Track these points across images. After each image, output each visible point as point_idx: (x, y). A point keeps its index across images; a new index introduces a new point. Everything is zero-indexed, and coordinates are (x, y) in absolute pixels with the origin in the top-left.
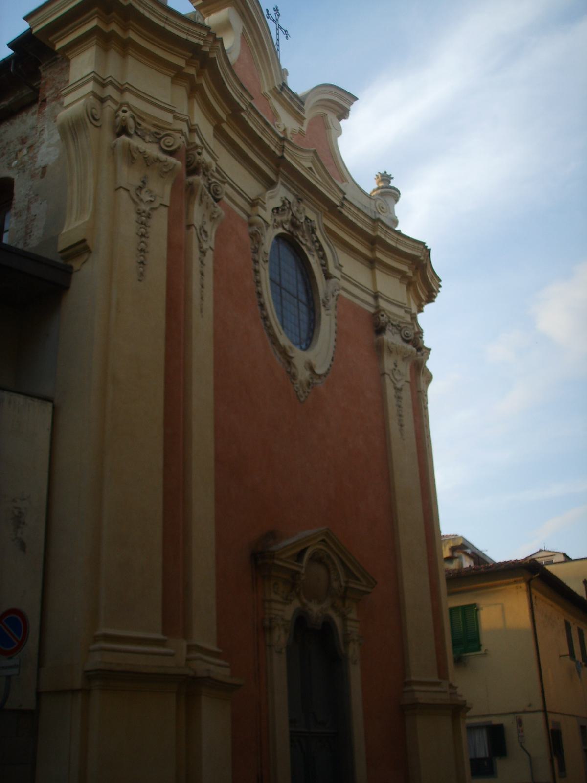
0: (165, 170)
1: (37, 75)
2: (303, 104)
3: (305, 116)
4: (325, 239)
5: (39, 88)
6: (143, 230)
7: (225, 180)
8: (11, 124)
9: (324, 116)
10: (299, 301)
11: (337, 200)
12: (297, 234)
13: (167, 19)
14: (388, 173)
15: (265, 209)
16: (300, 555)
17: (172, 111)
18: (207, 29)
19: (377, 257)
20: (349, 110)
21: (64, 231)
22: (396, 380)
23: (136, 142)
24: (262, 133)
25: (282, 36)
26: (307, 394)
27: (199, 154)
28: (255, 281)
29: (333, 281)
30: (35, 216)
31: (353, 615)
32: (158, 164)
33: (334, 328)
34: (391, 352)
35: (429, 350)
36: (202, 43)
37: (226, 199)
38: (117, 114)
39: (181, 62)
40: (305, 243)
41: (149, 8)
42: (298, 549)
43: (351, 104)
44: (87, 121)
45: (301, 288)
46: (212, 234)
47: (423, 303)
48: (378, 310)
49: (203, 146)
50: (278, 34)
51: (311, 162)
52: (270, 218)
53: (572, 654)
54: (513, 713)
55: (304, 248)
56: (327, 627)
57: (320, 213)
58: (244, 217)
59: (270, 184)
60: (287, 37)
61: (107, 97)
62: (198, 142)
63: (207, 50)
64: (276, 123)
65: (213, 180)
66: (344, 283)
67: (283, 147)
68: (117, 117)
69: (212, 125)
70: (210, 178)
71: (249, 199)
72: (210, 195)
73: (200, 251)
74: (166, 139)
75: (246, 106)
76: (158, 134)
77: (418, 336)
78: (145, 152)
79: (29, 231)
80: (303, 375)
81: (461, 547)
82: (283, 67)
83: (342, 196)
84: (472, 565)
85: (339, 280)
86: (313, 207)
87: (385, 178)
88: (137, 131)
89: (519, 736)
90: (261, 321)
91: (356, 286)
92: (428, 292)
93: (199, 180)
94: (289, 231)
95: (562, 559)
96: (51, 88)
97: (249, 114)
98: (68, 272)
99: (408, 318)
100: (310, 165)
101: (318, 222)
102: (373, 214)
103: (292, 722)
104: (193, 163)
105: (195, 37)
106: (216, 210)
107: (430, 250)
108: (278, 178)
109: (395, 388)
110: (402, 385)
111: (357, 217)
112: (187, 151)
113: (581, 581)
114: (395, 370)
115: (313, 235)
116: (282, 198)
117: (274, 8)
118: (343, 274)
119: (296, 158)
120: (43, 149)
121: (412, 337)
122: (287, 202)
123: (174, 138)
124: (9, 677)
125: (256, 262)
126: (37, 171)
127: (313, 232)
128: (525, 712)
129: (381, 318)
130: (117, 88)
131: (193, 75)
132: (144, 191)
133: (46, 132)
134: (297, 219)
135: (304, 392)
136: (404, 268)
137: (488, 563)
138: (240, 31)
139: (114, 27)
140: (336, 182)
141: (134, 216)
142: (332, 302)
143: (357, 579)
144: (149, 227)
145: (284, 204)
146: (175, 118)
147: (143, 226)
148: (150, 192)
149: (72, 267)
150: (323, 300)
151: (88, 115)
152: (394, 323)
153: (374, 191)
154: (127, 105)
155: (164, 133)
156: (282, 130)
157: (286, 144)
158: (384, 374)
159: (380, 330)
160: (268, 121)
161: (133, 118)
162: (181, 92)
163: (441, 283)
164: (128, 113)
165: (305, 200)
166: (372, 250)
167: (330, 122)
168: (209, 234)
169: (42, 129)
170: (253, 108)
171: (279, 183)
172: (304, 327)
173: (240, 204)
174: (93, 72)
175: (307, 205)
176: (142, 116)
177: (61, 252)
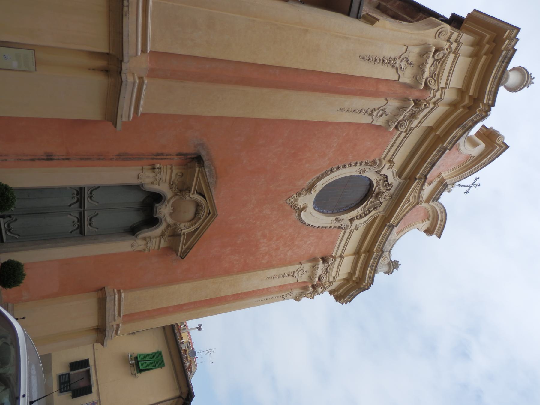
4: (371, 217)
6: (386, 61)
11: (393, 222)
14: (400, 267)
19: (362, 255)
24: (429, 162)
26: (291, 205)
27: (321, 289)
28: (351, 163)
35: (313, 299)
40: (368, 204)
54: (100, 400)
67: (421, 179)
69: (335, 288)
70: (409, 121)
71: (459, 39)
78: (427, 63)
83: (395, 225)
85: (350, 229)
86: (388, 206)
90: (330, 168)
94: (375, 191)
100: (411, 201)
106: (393, 123)
107: (369, 289)
109: (294, 272)
115: (372, 209)
118: (353, 230)
122: (390, 187)
129: (331, 259)
134: (381, 196)
136: (357, 274)
141: (393, 57)
142: (338, 225)
144: (388, 66)
145: (389, 185)
152: (328, 269)
154: (335, 261)
159: (325, 260)
166: (364, 252)
173: (389, 154)
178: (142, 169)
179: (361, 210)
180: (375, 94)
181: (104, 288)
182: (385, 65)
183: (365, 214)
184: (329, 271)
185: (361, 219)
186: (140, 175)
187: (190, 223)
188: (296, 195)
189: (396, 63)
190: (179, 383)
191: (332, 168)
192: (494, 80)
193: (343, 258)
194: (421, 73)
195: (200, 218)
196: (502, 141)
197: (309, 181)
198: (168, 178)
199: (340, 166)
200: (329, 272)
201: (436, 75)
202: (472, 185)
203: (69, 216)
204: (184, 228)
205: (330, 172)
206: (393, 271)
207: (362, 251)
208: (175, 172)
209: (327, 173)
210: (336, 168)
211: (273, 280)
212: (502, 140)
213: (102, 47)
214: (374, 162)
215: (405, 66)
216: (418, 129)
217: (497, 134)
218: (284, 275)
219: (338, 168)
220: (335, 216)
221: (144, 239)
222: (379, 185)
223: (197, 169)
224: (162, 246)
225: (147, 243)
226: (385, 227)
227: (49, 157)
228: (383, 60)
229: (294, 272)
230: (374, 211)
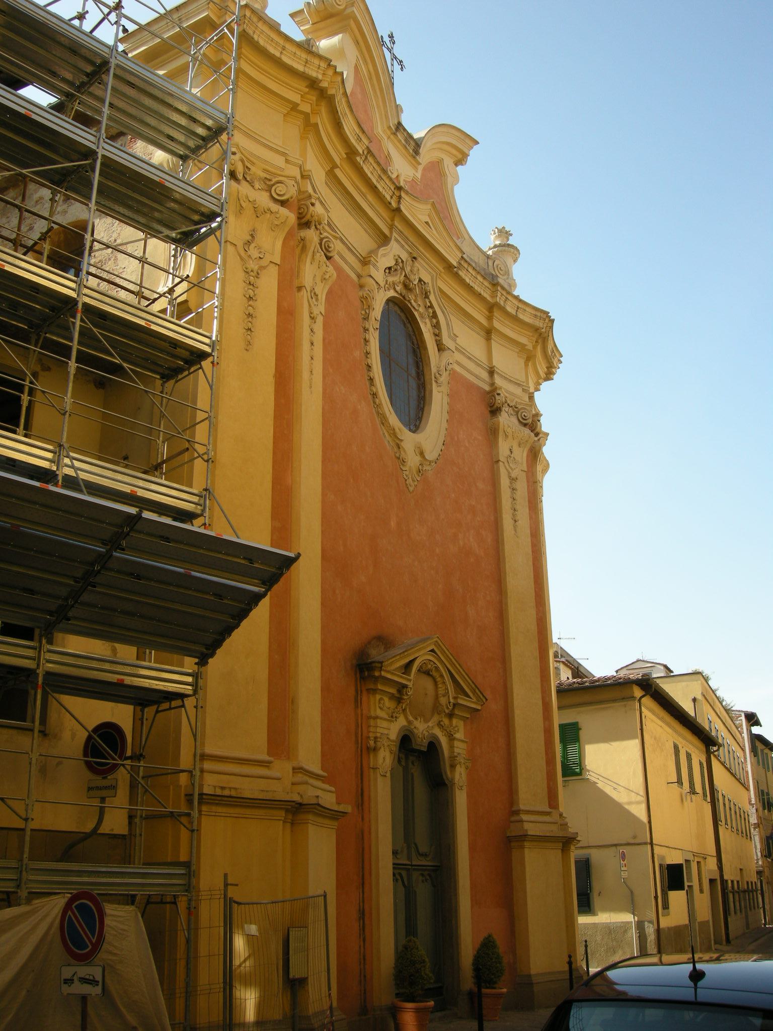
7: (337, 236)
12: (409, 298)
15: (377, 270)
16: (408, 666)
17: (284, 154)
26: (416, 483)
27: (313, 205)
29: (446, 354)
31: (459, 735)
32: (268, 215)
35: (547, 435)
36: (320, 77)
37: (337, 258)
45: (411, 360)
46: (322, 297)
48: (493, 391)
51: (429, 216)
53: (680, 782)
55: (416, 313)
56: (433, 746)
58: (353, 276)
62: (310, 190)
66: (458, 356)
69: (325, 170)
73: (311, 317)
74: (278, 187)
76: (270, 180)
77: (536, 419)
80: (413, 460)
82: (398, 103)
83: (460, 255)
91: (469, 358)
92: (547, 368)
93: (311, 234)
101: (433, 286)
103: (395, 853)
104: (306, 215)
107: (553, 321)
109: (510, 477)
112: (299, 201)
114: (510, 457)
115: (427, 300)
116: (395, 256)
121: (530, 421)
123: (287, 186)
125: (366, 330)
127: (427, 297)
128: (628, 844)
129: (497, 397)
132: (253, 245)
135: (413, 481)
136: (523, 340)
137: (594, 677)
138: (354, 62)
140: (454, 238)
141: (241, 275)
142: (444, 378)
143: (468, 696)
144: (257, 288)
146: (287, 161)
147: (251, 287)
148: (259, 248)
153: (490, 249)
155: (277, 179)
158: (498, 461)
159: (495, 411)
161: (242, 161)
167: (446, 166)
168: (319, 297)
171: (393, 238)
172: (413, 404)
175: (423, 266)
176: (252, 159)
182: (255, 295)
187: (440, 686)
188: (404, 472)
190: (614, 700)
195: (437, 668)
199: (368, 376)
201: (268, 177)
204: (447, 697)
224: (463, 738)
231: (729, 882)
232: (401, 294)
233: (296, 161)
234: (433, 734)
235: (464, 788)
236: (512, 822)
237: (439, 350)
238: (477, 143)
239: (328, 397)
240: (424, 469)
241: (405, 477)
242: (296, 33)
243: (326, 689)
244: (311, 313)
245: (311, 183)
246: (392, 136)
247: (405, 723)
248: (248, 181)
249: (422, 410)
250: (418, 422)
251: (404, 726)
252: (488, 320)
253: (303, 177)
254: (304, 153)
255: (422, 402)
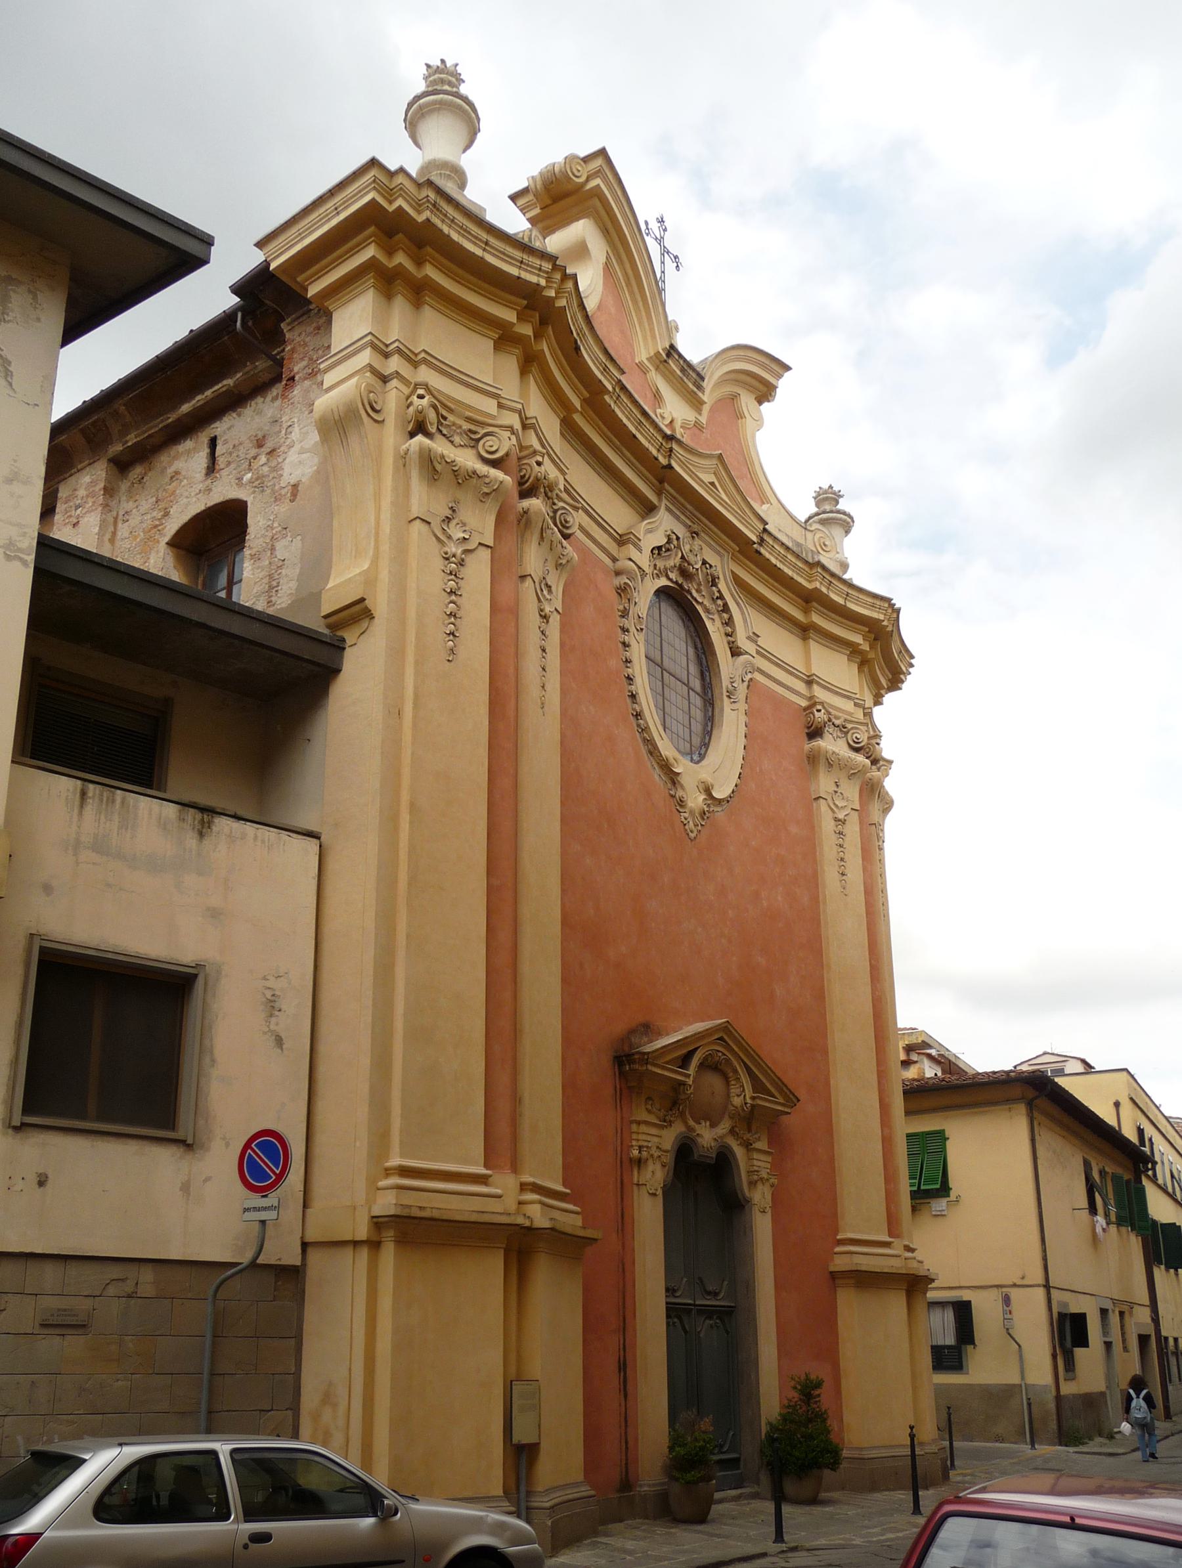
0: (486, 490)
1: (277, 338)
2: (703, 379)
3: (705, 398)
4: (732, 595)
5: (283, 359)
8: (239, 415)
9: (734, 397)
10: (690, 688)
13: (487, 243)
14: (836, 489)
15: (640, 551)
16: (685, 1061)
18: (552, 258)
19: (813, 622)
20: (777, 387)
21: (329, 586)
22: (837, 806)
23: (440, 446)
24: (636, 428)
25: (670, 265)
26: (699, 828)
30: (284, 560)
33: (743, 730)
34: (830, 765)
35: (890, 762)
36: (543, 282)
37: (579, 535)
38: (409, 401)
39: (509, 316)
40: (701, 599)
41: (459, 226)
42: (684, 1051)
43: (780, 376)
44: (363, 412)
45: (694, 669)
46: (558, 590)
47: (883, 692)
48: (813, 703)
49: (545, 451)
50: (663, 263)
52: (648, 563)
54: (998, 1286)
55: (699, 608)
56: (723, 1162)
57: (726, 554)
59: (648, 509)
60: (678, 266)
61: (391, 374)
63: (552, 294)
64: (659, 411)
65: (561, 504)
67: (671, 450)
68: (411, 404)
69: (558, 416)
70: (556, 501)
71: (615, 534)
72: (556, 529)
73: (541, 615)
75: (612, 384)
76: (475, 433)
79: (274, 583)
80: (696, 800)
81: (919, 1047)
84: (939, 1074)
87: (827, 498)
88: (440, 427)
89: (1004, 1319)
95: (1080, 1068)
96: (302, 359)
97: (617, 399)
98: (338, 647)
99: (859, 714)
100: (713, 478)
101: (723, 568)
102: (810, 555)
105: (530, 272)
107: (898, 611)
108: (660, 500)
109: (836, 820)
110: (846, 815)
111: (783, 559)
113: (1112, 1103)
115: (714, 588)
117: (657, 219)
119: (689, 465)
120: (292, 457)
123: (500, 440)
124: (263, 1222)
126: (283, 492)
127: (714, 584)
128: (1015, 1285)
130: (409, 360)
131: (530, 336)
132: (454, 522)
133: (296, 430)
134: (689, 564)
135: (696, 825)
136: (857, 639)
139: (400, 259)
141: (439, 563)
142: (742, 690)
144: (462, 579)
145: (669, 541)
146: (500, 406)
149: (344, 640)
150: (727, 688)
151: (363, 405)
152: (837, 722)
154: (426, 387)
156: (667, 422)
157: (675, 446)
159: (815, 733)
160: (646, 408)
161: (435, 407)
162: (510, 364)
163: (913, 661)
164: (426, 399)
165: (703, 534)
166: (806, 612)
167: (744, 409)
168: (554, 589)
169: (289, 424)
170: (623, 388)
171: (662, 511)
172: (697, 727)
174: (370, 333)
176: (449, 404)
177: (325, 617)
178: (638, 1185)
179: (713, 619)
180: (515, 611)
181: (831, 1272)
182: (459, 588)
183: (723, 611)
184: (842, 720)
185: (733, 622)
186: (651, 1192)
187: (733, 1083)
189: (454, 556)
191: (632, 714)
192: (491, 250)
193: (815, 677)
194: (475, 481)
195: (728, 1061)
196: (582, 163)
197: (657, 778)
198: (654, 1131)
199: (629, 691)
200: (846, 720)
201: (473, 428)
202: (660, 244)
203: (701, 1335)
205: (641, 721)
206: (844, 513)
207: (802, 620)
208: (643, 1115)
209: (642, 730)
210: (634, 703)
211: (850, 876)
212: (578, 163)
213: (352, 1247)
214: (622, 591)
215: (458, 526)
216: (568, 469)
217: (558, 177)
218: (841, 846)
219: (633, 696)
220: (722, 700)
221: (753, 1184)
222: (666, 569)
223: (650, 1067)
224: (766, 1148)
225: (762, 1179)
226: (760, 554)
227: (623, 1367)
228: (452, 592)
229: (836, 820)
230: (719, 586)
231: (1171, 1341)
232: (676, 583)
233: (514, 404)
234: (726, 1143)
235: (769, 1210)
236: (835, 1254)
237: (732, 656)
238: (787, 368)
239: (568, 717)
240: (711, 809)
241: (683, 820)
242: (514, 222)
243: (570, 1086)
244: (542, 610)
245: (537, 435)
246: (661, 366)
247: (683, 1129)
248: (444, 435)
249: (710, 734)
250: (703, 749)
251: (681, 1133)
252: (805, 613)
253: (525, 427)
254: (524, 392)
255: (710, 724)
